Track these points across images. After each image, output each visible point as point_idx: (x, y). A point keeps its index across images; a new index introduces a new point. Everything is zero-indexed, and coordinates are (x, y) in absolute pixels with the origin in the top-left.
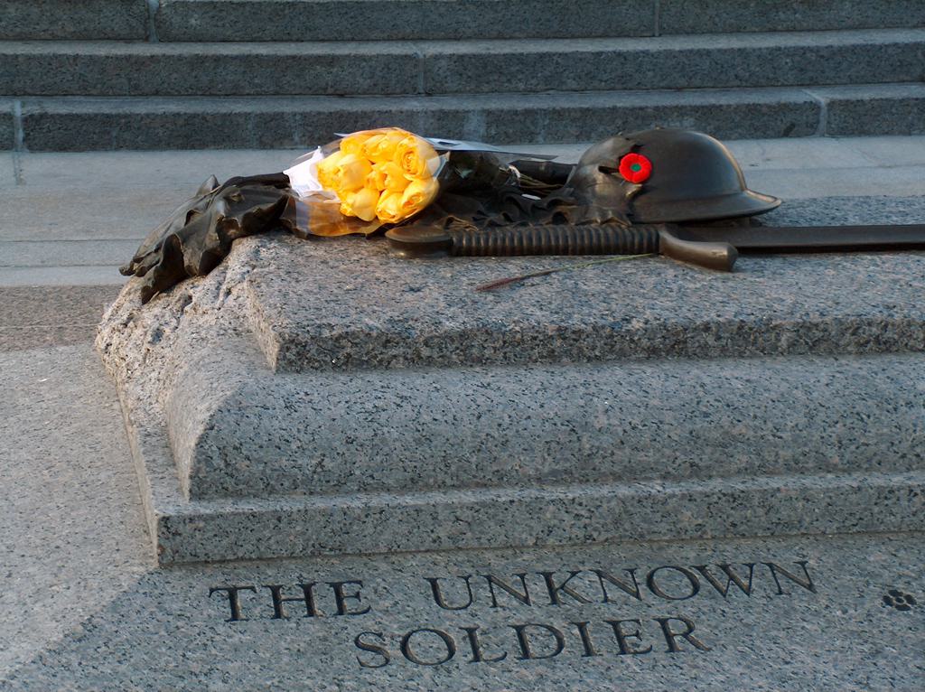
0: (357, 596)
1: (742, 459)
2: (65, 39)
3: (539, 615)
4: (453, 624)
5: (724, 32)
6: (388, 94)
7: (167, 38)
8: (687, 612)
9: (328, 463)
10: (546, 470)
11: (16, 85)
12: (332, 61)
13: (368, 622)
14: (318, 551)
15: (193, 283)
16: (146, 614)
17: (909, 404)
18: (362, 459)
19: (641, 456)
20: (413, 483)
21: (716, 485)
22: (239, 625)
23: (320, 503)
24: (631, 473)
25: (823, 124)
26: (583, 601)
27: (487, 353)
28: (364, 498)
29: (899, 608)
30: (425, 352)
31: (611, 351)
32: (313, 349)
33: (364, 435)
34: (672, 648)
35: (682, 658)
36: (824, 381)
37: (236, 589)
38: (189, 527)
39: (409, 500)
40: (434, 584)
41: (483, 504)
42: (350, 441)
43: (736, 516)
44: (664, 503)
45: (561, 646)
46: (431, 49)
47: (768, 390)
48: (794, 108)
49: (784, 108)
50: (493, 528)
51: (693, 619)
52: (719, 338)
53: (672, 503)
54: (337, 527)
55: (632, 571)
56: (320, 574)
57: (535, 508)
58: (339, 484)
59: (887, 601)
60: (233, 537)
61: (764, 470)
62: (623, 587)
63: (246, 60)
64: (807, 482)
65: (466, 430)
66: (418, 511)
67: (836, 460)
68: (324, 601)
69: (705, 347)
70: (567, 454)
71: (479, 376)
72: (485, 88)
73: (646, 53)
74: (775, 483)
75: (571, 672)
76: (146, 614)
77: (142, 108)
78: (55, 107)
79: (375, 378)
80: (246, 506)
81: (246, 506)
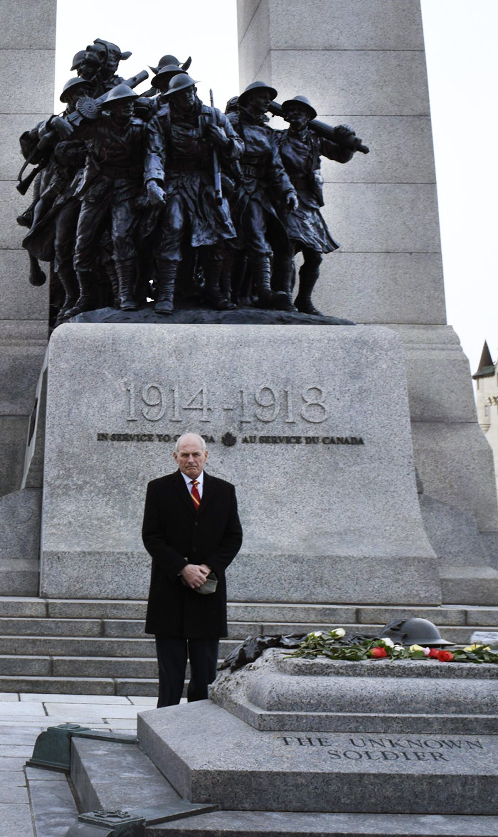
4: (361, 750)
9: (312, 701)
11: (111, 673)
15: (439, 408)
19: (419, 706)
27: (362, 672)
31: (405, 673)
34: (436, 759)
38: (269, 718)
40: (352, 740)
52: (441, 671)
69: (437, 674)
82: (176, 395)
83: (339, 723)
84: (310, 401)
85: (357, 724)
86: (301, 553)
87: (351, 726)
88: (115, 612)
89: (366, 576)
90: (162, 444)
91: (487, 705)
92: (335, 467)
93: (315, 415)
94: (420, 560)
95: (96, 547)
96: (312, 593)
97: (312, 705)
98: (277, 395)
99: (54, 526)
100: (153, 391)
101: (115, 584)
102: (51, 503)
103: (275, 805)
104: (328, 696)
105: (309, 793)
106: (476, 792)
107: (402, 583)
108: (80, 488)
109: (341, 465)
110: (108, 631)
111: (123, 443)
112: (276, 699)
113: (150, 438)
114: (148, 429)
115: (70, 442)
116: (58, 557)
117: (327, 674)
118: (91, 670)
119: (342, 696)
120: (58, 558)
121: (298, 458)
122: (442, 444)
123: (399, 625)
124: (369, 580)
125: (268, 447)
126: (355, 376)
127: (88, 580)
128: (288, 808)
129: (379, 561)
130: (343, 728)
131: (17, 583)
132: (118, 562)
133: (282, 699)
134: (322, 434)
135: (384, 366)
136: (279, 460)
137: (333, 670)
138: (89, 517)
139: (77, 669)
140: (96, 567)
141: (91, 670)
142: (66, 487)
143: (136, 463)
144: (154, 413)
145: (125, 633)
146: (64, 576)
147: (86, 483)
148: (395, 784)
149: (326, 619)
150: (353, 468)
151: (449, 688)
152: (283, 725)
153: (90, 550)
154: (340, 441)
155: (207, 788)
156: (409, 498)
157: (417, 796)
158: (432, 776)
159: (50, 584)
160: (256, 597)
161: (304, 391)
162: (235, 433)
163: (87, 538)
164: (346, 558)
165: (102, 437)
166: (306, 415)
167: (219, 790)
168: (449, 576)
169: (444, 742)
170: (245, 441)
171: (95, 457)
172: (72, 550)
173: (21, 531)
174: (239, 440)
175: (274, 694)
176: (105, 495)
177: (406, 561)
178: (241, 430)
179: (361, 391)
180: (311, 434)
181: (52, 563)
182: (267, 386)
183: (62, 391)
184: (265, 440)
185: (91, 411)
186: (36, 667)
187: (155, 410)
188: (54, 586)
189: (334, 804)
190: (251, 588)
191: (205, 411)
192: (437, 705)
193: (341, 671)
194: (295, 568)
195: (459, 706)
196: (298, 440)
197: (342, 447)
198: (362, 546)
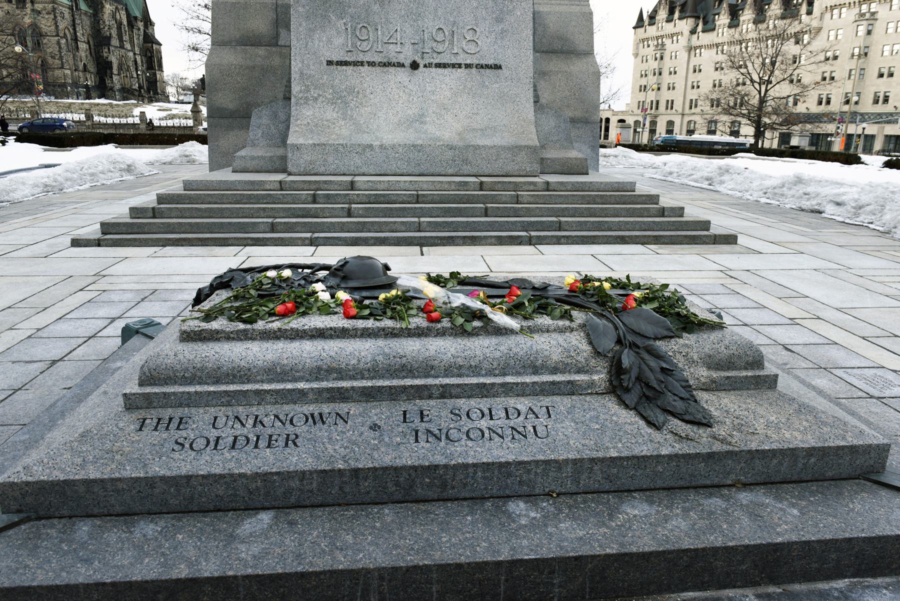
17: (394, 357)
35: (288, 450)
38: (133, 397)
82: (379, 33)
83: (210, 398)
84: (468, 38)
85: (229, 398)
86: (455, 143)
87: (223, 400)
89: (494, 158)
90: (370, 68)
91: (369, 370)
92: (483, 85)
93: (472, 48)
94: (528, 147)
95: (323, 140)
96: (460, 169)
97: (186, 378)
98: (447, 33)
99: (297, 126)
100: (363, 30)
102: (296, 110)
103: (96, 511)
104: (202, 369)
105: (132, 496)
106: (314, 485)
108: (316, 99)
109: (487, 83)
110: (318, 199)
111: (344, 67)
112: (147, 374)
113: (362, 64)
114: (361, 57)
115: (308, 66)
116: (297, 147)
117: (218, 340)
118: (299, 229)
119: (219, 368)
121: (459, 78)
122: (572, 67)
125: (440, 70)
126: (499, 20)
128: (111, 512)
129: (503, 148)
130: (214, 402)
132: (337, 150)
133: (154, 373)
134: (476, 62)
135: (519, 13)
136: (447, 80)
138: (322, 120)
139: (290, 228)
141: (299, 229)
142: (307, 98)
143: (353, 82)
144: (365, 46)
147: (319, 95)
148: (226, 483)
149: (461, 188)
150: (495, 86)
151: (333, 354)
152: (151, 403)
154: (488, 67)
155: (15, 499)
156: (527, 106)
157: (251, 493)
158: (266, 474)
159: (293, 166)
160: (425, 172)
161: (465, 31)
162: (419, 60)
163: (319, 134)
164: (483, 146)
165: (330, 63)
166: (466, 48)
167: (29, 500)
168: (549, 156)
169: (312, 415)
170: (425, 66)
171: (325, 77)
172: (306, 143)
174: (421, 65)
176: (332, 104)
177: (520, 148)
178: (423, 58)
179: (503, 31)
180: (468, 62)
182: (441, 26)
183: (301, 29)
184: (438, 65)
185: (321, 44)
186: (262, 227)
187: (365, 43)
189: (161, 505)
191: (399, 45)
192: (318, 372)
193: (232, 336)
194: (450, 153)
195: (340, 373)
196: (460, 66)
197: (488, 71)
198: (494, 138)
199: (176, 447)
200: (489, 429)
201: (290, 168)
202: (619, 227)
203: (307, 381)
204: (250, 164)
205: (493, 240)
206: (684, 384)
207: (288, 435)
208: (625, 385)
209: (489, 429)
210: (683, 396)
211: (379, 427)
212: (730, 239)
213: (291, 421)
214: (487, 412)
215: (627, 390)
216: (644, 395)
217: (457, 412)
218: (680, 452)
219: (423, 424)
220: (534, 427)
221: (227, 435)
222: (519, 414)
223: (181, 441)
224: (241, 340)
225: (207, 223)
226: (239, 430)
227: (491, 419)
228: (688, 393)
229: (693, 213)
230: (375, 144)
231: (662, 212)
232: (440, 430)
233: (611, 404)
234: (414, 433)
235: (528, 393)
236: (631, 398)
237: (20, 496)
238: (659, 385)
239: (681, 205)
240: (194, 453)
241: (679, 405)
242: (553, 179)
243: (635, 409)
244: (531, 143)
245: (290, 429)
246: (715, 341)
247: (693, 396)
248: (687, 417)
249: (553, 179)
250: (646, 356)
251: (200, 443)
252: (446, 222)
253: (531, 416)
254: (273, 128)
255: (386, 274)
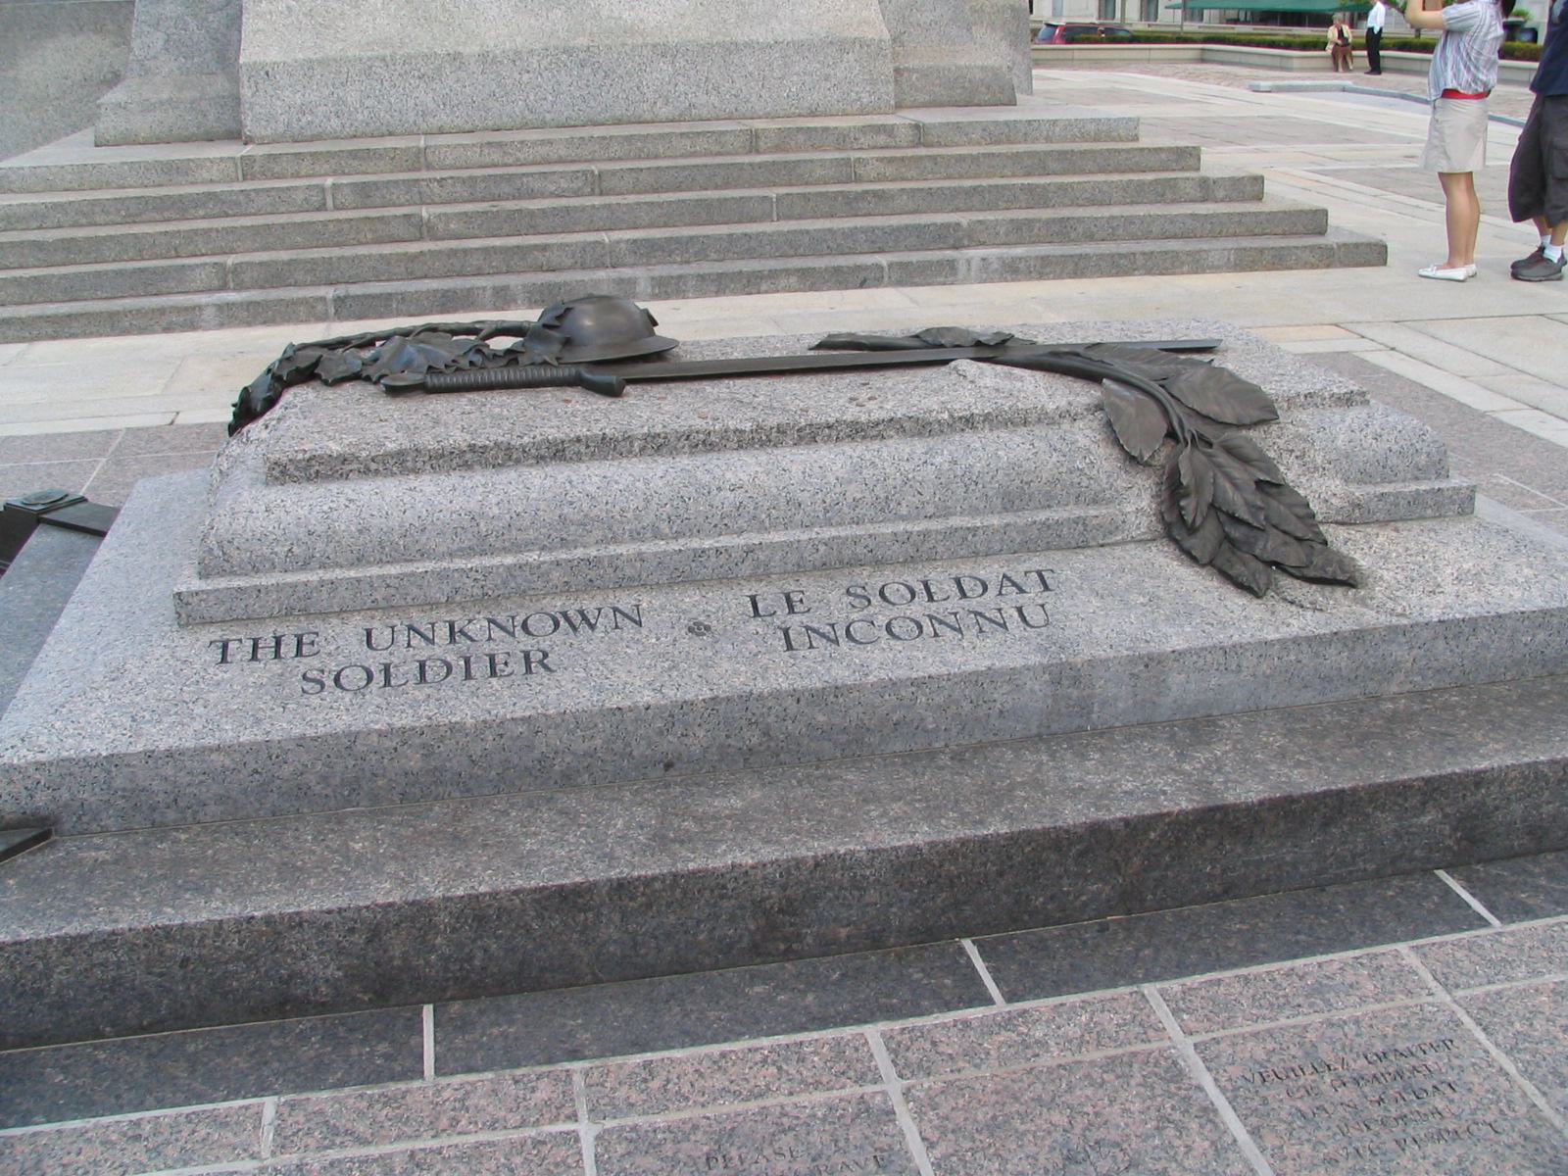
0: (312, 643)
1: (598, 534)
2: (367, 243)
3: (438, 651)
5: (822, 217)
6: (584, 267)
7: (435, 238)
8: (545, 645)
10: (455, 547)
11: (332, 277)
12: (545, 248)
13: (315, 662)
14: (289, 613)
16: (162, 660)
17: (719, 489)
18: (320, 546)
20: (360, 560)
21: (579, 553)
22: (224, 667)
23: (290, 578)
24: (516, 548)
25: (886, 279)
26: (472, 640)
27: (419, 465)
28: (321, 572)
29: (698, 635)
30: (373, 466)
32: (291, 468)
33: (320, 529)
35: (534, 679)
36: (660, 474)
37: (228, 641)
39: (352, 574)
41: (405, 575)
42: (310, 533)
43: (592, 575)
44: (539, 567)
45: (448, 673)
46: (616, 235)
47: (617, 483)
48: (866, 268)
49: (858, 268)
50: (415, 591)
51: (548, 649)
52: (588, 447)
53: (544, 567)
54: (301, 595)
55: (513, 618)
56: (289, 631)
57: (443, 576)
58: (306, 564)
59: (691, 630)
60: (228, 605)
61: (615, 540)
62: (503, 628)
63: (486, 250)
64: (644, 548)
65: (394, 522)
66: (359, 581)
67: (667, 530)
68: (288, 648)
70: (470, 536)
71: (412, 481)
72: (654, 261)
73: (764, 233)
74: (622, 549)
75: (450, 692)
76: (162, 660)
77: (413, 286)
78: (356, 290)
79: (334, 487)
80: (237, 582)
81: (237, 582)
88: (355, 163)
89: (777, 73)
94: (863, 43)
101: (366, 113)
107: (834, 81)
120: (267, 73)
123: (559, 318)
124: (782, 78)
127: (322, 108)
131: (211, 118)
137: (355, 466)
140: (333, 85)
145: (368, 202)
146: (279, 103)
153: (319, 56)
164: (746, 45)
169: (565, 615)
173: (215, 26)
175: (212, 542)
177: (843, 46)
181: (257, 84)
188: (263, 123)
190: (592, 104)
199: (308, 686)
200: (931, 617)
201: (250, 127)
202: (1113, 230)
203: (543, 548)
204: (142, 124)
205: (793, 280)
206: (1301, 511)
207: (527, 656)
208: (1189, 519)
209: (931, 617)
210: (1299, 535)
211: (708, 628)
212: (1374, 254)
213: (525, 626)
214: (919, 588)
215: (1192, 530)
216: (1227, 537)
217: (859, 591)
218: (1302, 634)
219: (797, 618)
220: (1020, 610)
221: (404, 658)
222: (985, 589)
223: (315, 674)
224: (393, 474)
225: (64, 277)
226: (423, 651)
227: (931, 598)
228: (1306, 532)
229: (1286, 190)
230: (466, 50)
231: (1207, 189)
232: (832, 626)
233: (1165, 561)
234: (780, 634)
235: (997, 547)
236: (1200, 544)
237: (25, 793)
238: (1253, 515)
239: (1256, 171)
240: (348, 696)
241: (1293, 555)
242: (929, 117)
243: (1211, 563)
244: (870, 34)
245: (525, 642)
246: (1355, 426)
247: (1319, 533)
248: (1311, 573)
249: (929, 117)
250: (1222, 458)
251: (354, 677)
252: (677, 240)
253: (1009, 589)
254: (192, 25)
255: (652, 333)
